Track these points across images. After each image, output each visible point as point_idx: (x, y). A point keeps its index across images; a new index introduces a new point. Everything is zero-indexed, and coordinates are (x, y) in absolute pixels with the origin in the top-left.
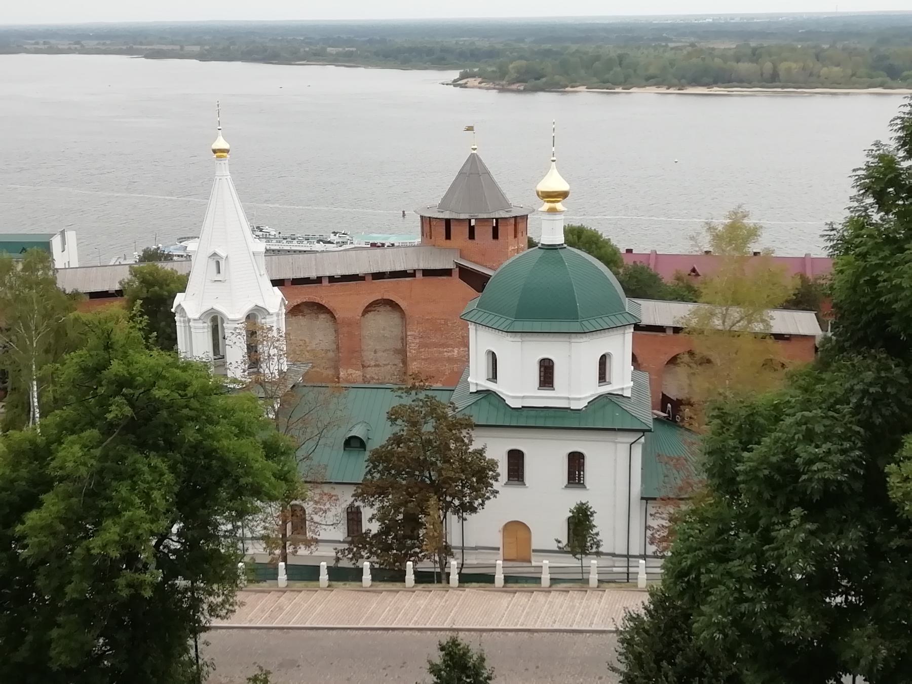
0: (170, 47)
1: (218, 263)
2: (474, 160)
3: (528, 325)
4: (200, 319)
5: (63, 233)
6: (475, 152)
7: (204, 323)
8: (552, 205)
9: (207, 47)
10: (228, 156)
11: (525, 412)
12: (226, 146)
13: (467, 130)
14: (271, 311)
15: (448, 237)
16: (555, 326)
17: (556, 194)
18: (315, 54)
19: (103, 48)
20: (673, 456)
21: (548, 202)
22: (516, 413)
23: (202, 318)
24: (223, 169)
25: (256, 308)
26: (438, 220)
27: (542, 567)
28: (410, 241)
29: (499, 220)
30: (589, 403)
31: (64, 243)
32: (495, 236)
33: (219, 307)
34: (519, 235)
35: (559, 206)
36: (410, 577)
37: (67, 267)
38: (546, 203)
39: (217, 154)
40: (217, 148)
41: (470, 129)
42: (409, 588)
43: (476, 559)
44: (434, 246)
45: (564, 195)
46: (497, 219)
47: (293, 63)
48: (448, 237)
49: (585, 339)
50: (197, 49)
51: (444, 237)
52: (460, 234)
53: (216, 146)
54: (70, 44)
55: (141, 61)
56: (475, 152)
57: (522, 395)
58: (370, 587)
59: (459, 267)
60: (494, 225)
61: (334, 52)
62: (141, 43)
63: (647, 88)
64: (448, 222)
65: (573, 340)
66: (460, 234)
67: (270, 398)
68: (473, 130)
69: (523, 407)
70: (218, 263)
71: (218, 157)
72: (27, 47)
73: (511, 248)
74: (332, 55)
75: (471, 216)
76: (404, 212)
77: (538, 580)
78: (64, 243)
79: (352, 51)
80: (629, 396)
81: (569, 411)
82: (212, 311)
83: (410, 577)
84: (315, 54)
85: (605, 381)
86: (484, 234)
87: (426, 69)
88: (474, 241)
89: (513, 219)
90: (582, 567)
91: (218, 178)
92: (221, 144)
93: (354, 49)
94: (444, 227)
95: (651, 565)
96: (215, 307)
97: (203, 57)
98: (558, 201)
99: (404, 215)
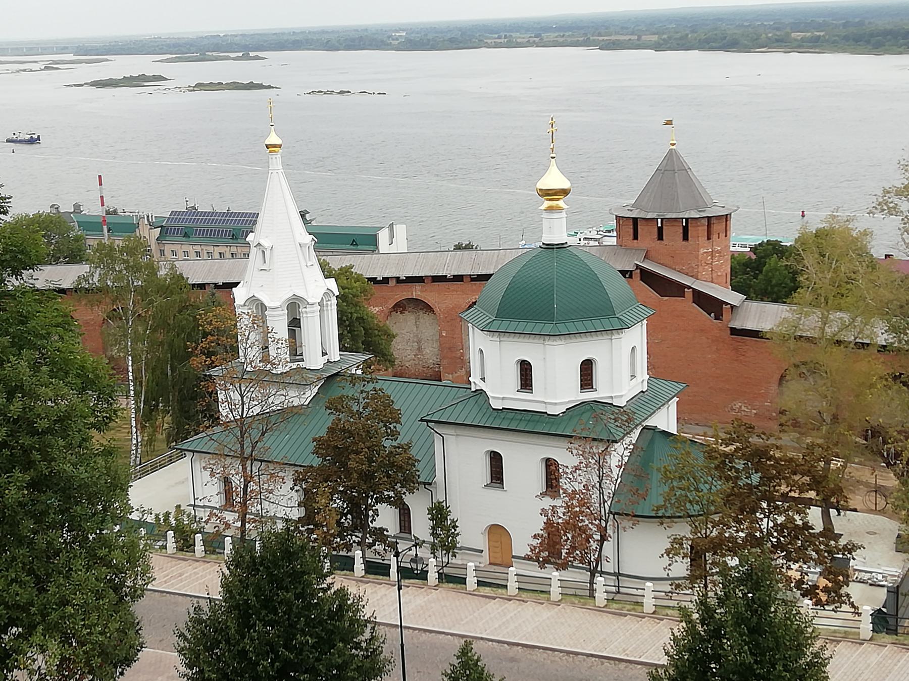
0: (627, 38)
1: (263, 252)
2: (672, 156)
3: (513, 326)
4: (245, 305)
5: (391, 226)
6: (674, 147)
8: (551, 203)
9: (665, 36)
10: (281, 151)
12: (278, 141)
13: (666, 124)
14: (310, 301)
15: (636, 237)
16: (529, 327)
17: (554, 192)
18: (777, 41)
19: (561, 40)
21: (547, 200)
22: (495, 413)
23: (247, 304)
24: (276, 161)
26: (625, 219)
27: (551, 579)
28: (742, 243)
29: (713, 221)
30: (567, 409)
31: (392, 236)
32: (686, 237)
34: (714, 237)
35: (561, 203)
36: (359, 566)
37: (296, 255)
38: (546, 201)
39: (269, 149)
41: (669, 123)
42: (470, 591)
43: (461, 559)
44: (621, 246)
45: (565, 192)
46: (687, 219)
47: (752, 50)
48: (636, 237)
49: (559, 342)
50: (655, 38)
51: (632, 237)
52: (647, 235)
53: (269, 141)
54: (531, 37)
55: (596, 52)
56: (674, 147)
57: (502, 396)
58: (652, 614)
59: (640, 269)
60: (684, 224)
61: (799, 38)
62: (600, 35)
64: (635, 220)
65: (547, 343)
66: (647, 235)
68: (672, 124)
69: (503, 408)
70: (263, 252)
71: (270, 152)
72: (489, 41)
73: (702, 251)
74: (796, 40)
75: (659, 215)
76: (803, 212)
77: (463, 581)
78: (392, 236)
79: (820, 36)
81: (546, 415)
83: (359, 566)
84: (777, 41)
85: (592, 388)
86: (673, 235)
87: (900, 53)
88: (662, 242)
89: (706, 219)
90: (619, 587)
93: (822, 34)
94: (632, 227)
95: (505, 575)
97: (658, 47)
98: (558, 199)
99: (803, 216)
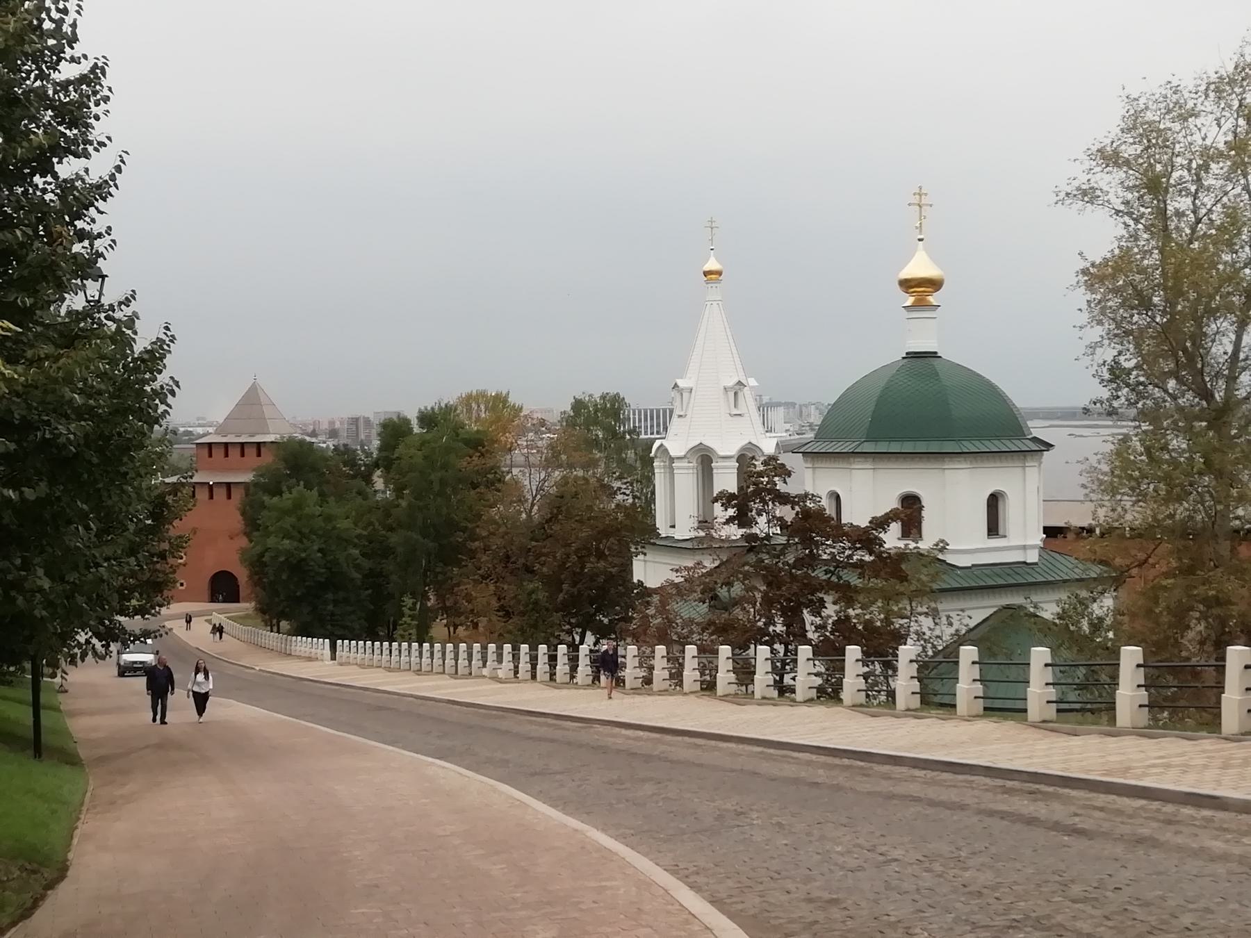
7: (689, 462)
11: (974, 569)
20: (995, 442)
23: (688, 456)
25: (749, 446)
33: (708, 442)
40: (708, 270)
53: (707, 267)
63: (1189, 807)
67: (828, 680)
69: (973, 565)
80: (1036, 560)
82: (701, 447)
91: (709, 303)
92: (712, 265)
96: (704, 442)
